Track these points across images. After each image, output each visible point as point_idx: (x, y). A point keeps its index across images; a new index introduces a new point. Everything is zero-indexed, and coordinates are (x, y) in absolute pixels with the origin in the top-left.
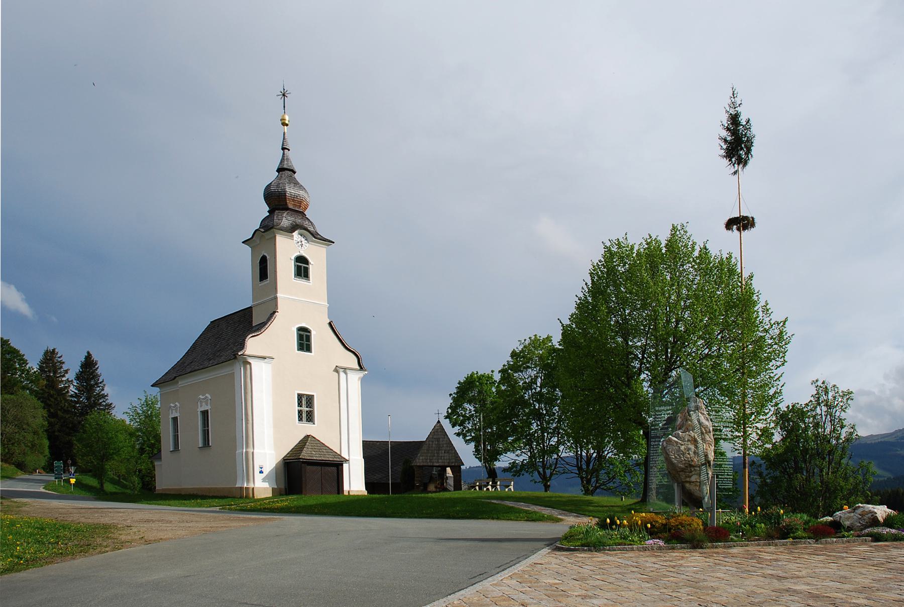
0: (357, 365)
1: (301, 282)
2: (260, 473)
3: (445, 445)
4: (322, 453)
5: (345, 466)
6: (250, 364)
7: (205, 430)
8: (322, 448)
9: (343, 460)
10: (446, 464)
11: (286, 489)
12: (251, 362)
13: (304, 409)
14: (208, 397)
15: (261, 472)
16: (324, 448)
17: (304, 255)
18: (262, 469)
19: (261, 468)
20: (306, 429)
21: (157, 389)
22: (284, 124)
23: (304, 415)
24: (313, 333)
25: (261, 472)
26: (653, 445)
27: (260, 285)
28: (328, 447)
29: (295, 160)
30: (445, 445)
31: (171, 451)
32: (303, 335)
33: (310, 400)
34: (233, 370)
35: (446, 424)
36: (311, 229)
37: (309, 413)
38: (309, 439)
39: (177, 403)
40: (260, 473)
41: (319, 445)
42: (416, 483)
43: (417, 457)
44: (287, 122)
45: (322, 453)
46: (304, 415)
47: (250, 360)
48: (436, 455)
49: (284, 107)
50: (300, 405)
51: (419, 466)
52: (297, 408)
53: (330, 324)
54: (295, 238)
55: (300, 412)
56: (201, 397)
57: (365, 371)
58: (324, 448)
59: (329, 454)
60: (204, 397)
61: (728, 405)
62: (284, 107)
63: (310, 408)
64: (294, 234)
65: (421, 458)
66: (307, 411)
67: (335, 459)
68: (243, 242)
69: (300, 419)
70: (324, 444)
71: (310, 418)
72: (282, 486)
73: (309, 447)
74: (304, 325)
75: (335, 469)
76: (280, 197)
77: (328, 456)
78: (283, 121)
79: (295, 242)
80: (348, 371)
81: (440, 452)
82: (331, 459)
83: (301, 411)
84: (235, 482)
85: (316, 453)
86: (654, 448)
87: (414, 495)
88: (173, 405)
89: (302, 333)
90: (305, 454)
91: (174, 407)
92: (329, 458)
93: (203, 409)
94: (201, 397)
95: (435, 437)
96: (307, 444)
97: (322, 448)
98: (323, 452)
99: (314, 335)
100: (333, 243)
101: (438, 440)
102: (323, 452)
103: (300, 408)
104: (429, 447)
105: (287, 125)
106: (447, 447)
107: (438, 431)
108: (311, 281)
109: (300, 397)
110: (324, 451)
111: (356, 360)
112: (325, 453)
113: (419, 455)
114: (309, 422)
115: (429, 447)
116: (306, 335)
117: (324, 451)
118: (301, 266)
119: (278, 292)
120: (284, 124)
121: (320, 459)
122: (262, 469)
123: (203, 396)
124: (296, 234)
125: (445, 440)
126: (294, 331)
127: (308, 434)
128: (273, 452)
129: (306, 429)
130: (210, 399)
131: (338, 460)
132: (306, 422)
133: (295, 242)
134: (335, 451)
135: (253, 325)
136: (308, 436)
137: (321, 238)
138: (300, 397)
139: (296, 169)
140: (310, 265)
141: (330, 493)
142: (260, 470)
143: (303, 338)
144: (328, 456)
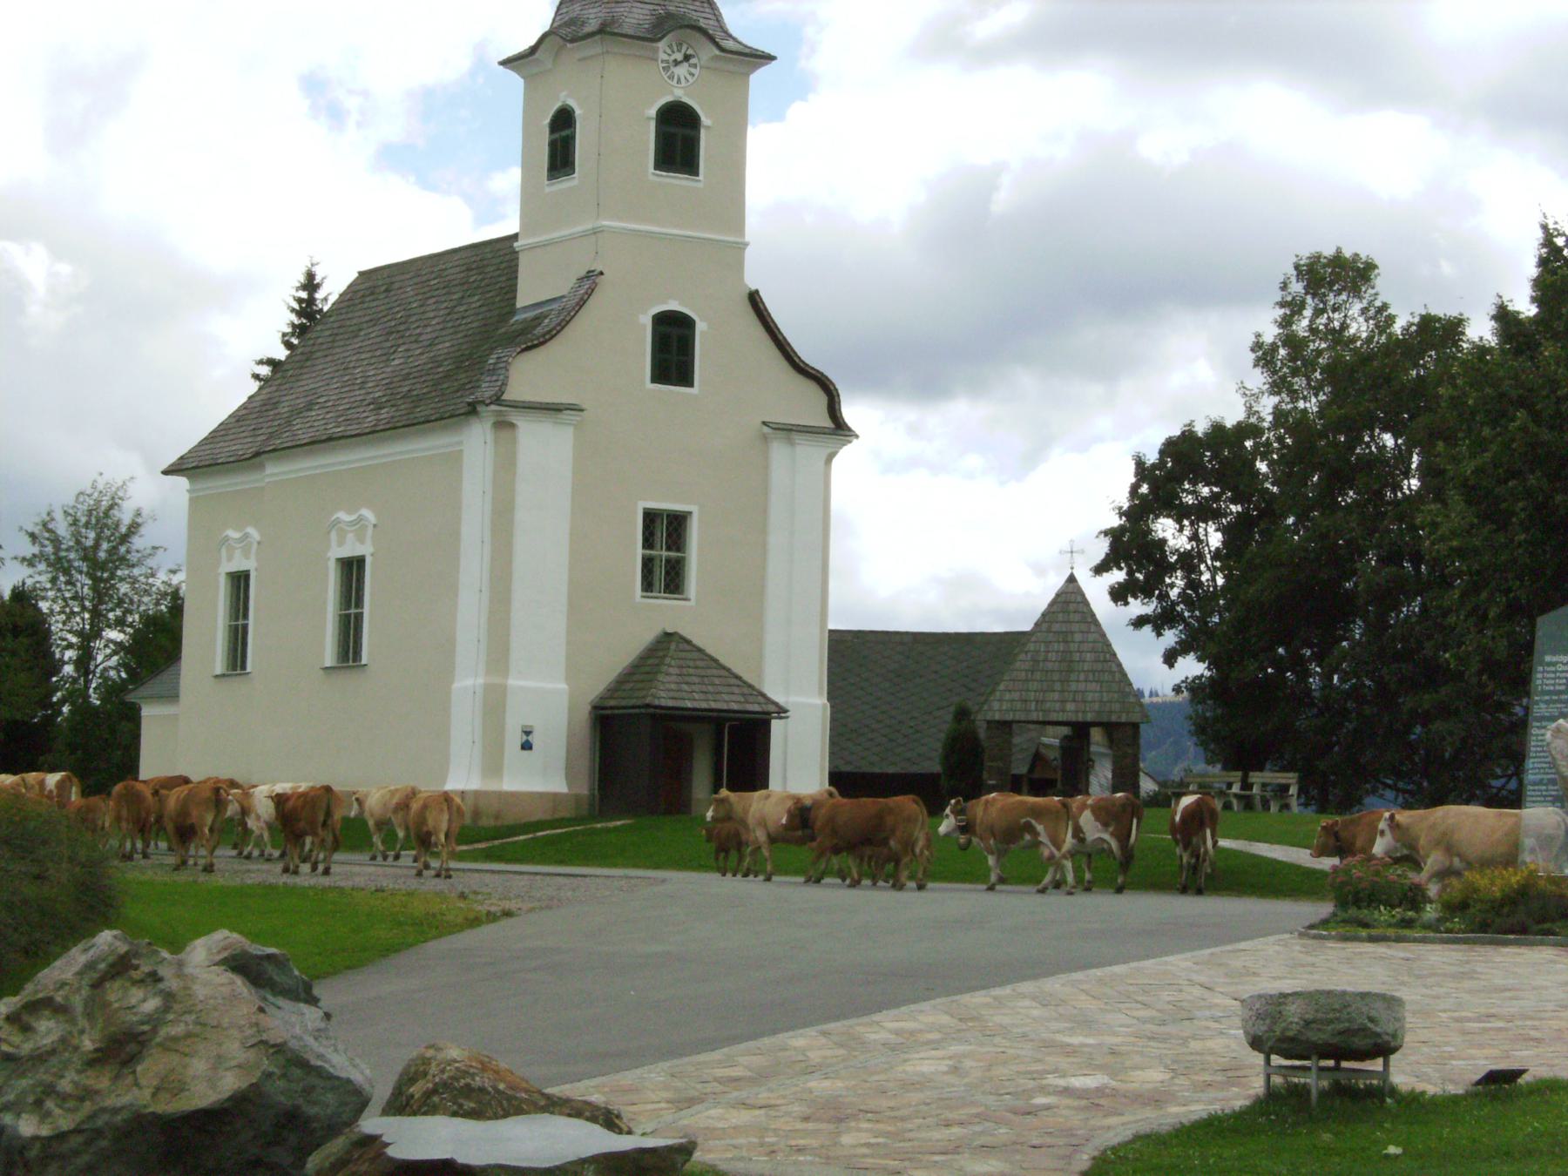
0: (826, 415)
1: (677, 181)
3: (1089, 656)
4: (710, 688)
5: (776, 725)
6: (512, 426)
7: (348, 616)
8: (709, 672)
9: (771, 708)
10: (1089, 717)
12: (514, 422)
14: (367, 520)
15: (527, 746)
16: (715, 672)
17: (686, 100)
18: (530, 738)
20: (665, 614)
21: (182, 482)
23: (659, 574)
24: (701, 327)
25: (527, 746)
26: (1537, 735)
27: (547, 190)
28: (729, 670)
30: (1089, 656)
31: (217, 676)
34: (460, 443)
35: (1096, 591)
38: (673, 646)
39: (251, 530)
42: (985, 775)
43: (994, 691)
45: (710, 688)
48: (1058, 686)
50: (648, 542)
51: (998, 722)
52: (639, 551)
55: (648, 563)
56: (344, 516)
60: (353, 517)
63: (678, 550)
65: (1007, 696)
69: (648, 585)
70: (716, 661)
72: (583, 789)
73: (671, 670)
74: (673, 305)
76: (1072, 607)
77: (726, 697)
79: (661, 65)
81: (1073, 676)
85: (694, 687)
86: (1537, 741)
87: (599, 826)
88: (236, 535)
90: (668, 693)
91: (240, 540)
92: (729, 702)
93: (347, 552)
94: (344, 516)
95: (1056, 627)
96: (668, 660)
97: (709, 672)
98: (713, 684)
99: (702, 332)
101: (1065, 637)
102: (713, 684)
104: (1036, 661)
106: (1097, 661)
107: (1069, 600)
108: (701, 177)
109: (650, 517)
110: (717, 681)
111: (822, 399)
113: (1002, 687)
114: (671, 592)
115: (1036, 661)
117: (717, 681)
122: (530, 738)
123: (349, 512)
125: (1091, 637)
126: (644, 326)
127: (670, 630)
128: (563, 686)
129: (665, 614)
130: (375, 526)
132: (662, 595)
133: (661, 65)
134: (750, 681)
135: (520, 303)
136: (668, 637)
137: (747, 51)
138: (650, 517)
142: (525, 738)
144: (726, 697)
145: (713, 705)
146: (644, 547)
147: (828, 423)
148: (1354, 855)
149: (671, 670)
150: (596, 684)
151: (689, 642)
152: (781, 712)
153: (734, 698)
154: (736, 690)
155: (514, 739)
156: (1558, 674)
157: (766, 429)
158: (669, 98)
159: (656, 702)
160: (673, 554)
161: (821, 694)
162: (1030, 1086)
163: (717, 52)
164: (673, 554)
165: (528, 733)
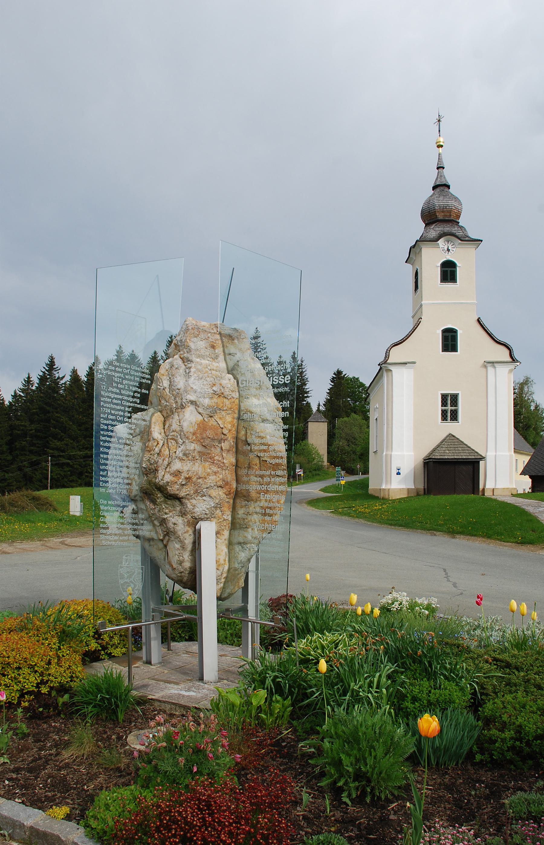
1: (449, 286)
2: (397, 474)
4: (457, 452)
5: (482, 463)
6: (391, 370)
11: (424, 489)
13: (449, 408)
15: (398, 474)
16: (461, 446)
17: (451, 259)
19: (399, 469)
22: (440, 146)
23: (449, 414)
25: (398, 474)
28: (466, 445)
29: (449, 176)
32: (448, 336)
33: (454, 398)
36: (460, 233)
37: (453, 412)
40: (397, 474)
41: (456, 443)
44: (441, 144)
45: (457, 452)
46: (449, 414)
47: (391, 367)
49: (439, 131)
50: (444, 403)
52: (440, 408)
53: (479, 321)
54: (441, 246)
57: (517, 361)
58: (461, 446)
59: (464, 451)
61: (294, 835)
62: (439, 131)
63: (455, 406)
64: (438, 242)
66: (451, 410)
67: (470, 457)
68: (406, 262)
69: (444, 417)
71: (454, 417)
72: (421, 486)
75: (470, 467)
78: (438, 144)
80: (495, 365)
82: (464, 457)
83: (445, 410)
84: (381, 484)
89: (447, 334)
92: (464, 456)
99: (460, 334)
100: (482, 241)
103: (444, 408)
105: (442, 146)
108: (458, 283)
109: (444, 397)
112: (461, 451)
116: (452, 336)
118: (447, 271)
119: (423, 299)
120: (440, 146)
121: (452, 457)
124: (441, 242)
128: (413, 453)
129: (450, 427)
131: (473, 457)
138: (444, 397)
139: (450, 183)
140: (458, 268)
141: (465, 492)
143: (448, 339)
145: (456, 457)
146: (442, 406)
147: (511, 360)
148: (341, 757)
149: (444, 446)
150: (424, 453)
151: (454, 436)
152: (483, 458)
153: (465, 454)
154: (467, 451)
155: (394, 471)
156: (132, 394)
157: (486, 364)
158: (445, 259)
159: (434, 457)
160: (453, 408)
161: (509, 450)
162: (344, 755)
163: (460, 242)
164: (453, 408)
165: (399, 469)
